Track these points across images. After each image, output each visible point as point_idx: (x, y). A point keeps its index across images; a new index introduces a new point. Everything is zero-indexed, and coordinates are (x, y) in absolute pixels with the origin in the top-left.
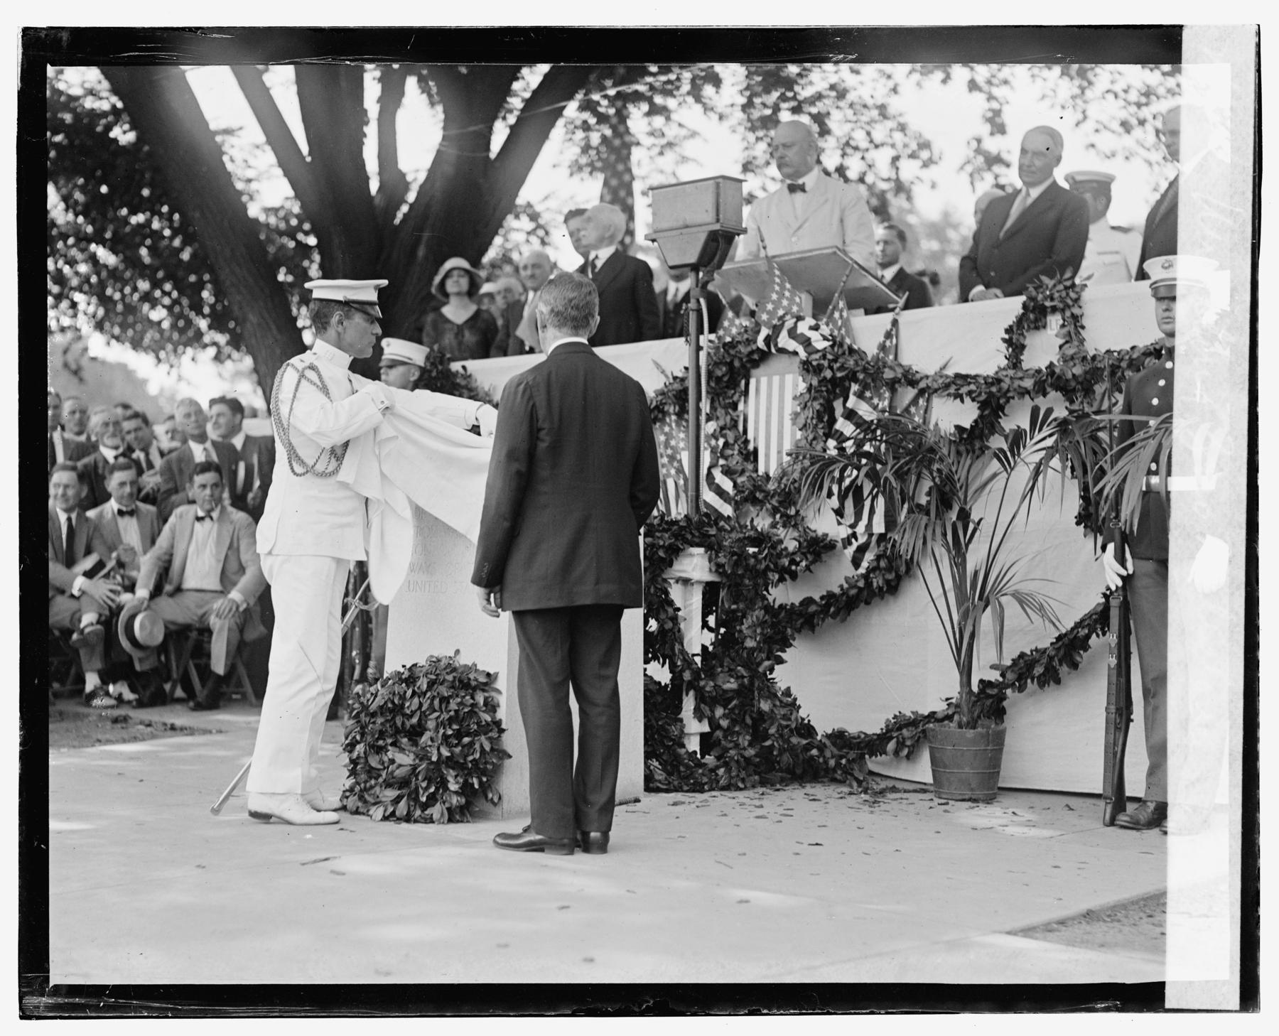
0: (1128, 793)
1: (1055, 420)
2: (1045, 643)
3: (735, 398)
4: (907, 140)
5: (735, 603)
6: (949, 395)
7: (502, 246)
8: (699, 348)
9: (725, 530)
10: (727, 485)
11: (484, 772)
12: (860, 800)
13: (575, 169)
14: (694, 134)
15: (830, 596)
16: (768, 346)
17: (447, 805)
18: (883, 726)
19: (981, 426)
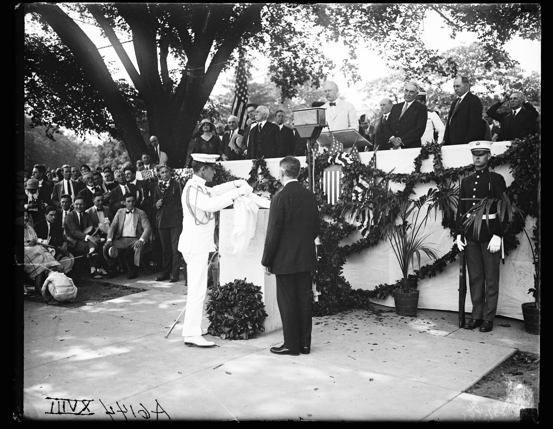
3: (319, 178)
15: (354, 245)
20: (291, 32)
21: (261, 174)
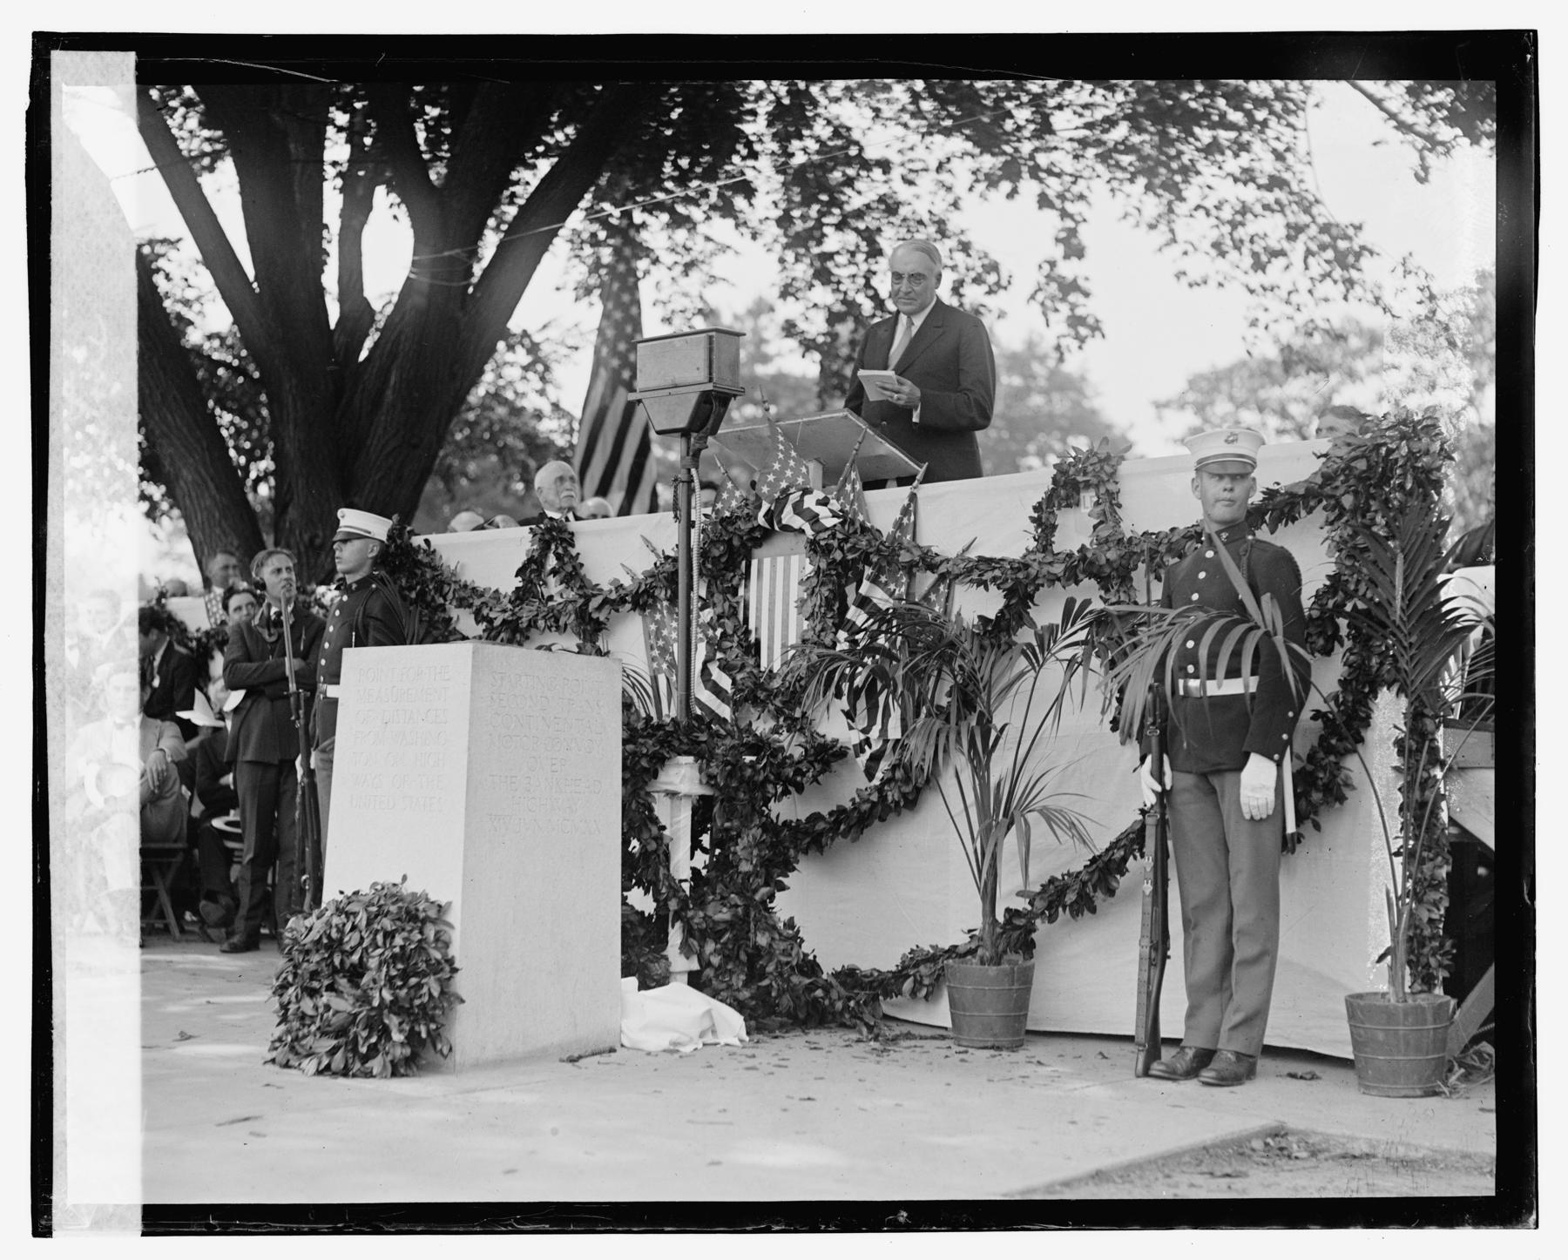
0: (1164, 1034)
2: (1078, 866)
3: (735, 582)
4: (970, 262)
5: (728, 820)
6: (970, 581)
8: (691, 524)
9: (719, 736)
10: (725, 682)
12: (868, 1049)
13: (581, 292)
15: (840, 812)
17: (390, 1058)
18: (899, 962)
19: (1007, 616)
20: (849, 161)
21: (554, 572)
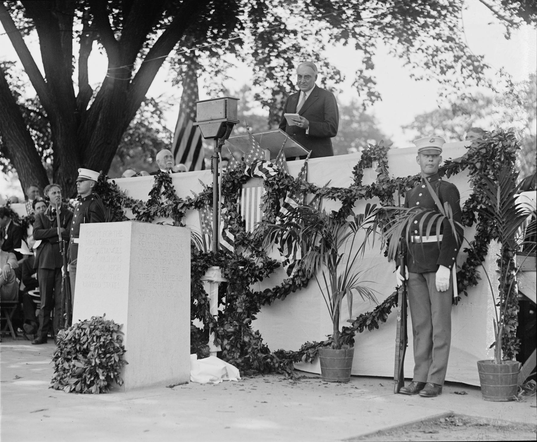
1: (376, 209)
2: (371, 310)
3: (235, 197)
4: (329, 70)
5: (233, 292)
7: (140, 119)
8: (218, 175)
9: (229, 258)
10: (232, 237)
11: (116, 371)
12: (288, 382)
13: (175, 82)
14: (231, 65)
16: (250, 174)
18: (300, 348)
20: (281, 31)
21: (164, 193)
